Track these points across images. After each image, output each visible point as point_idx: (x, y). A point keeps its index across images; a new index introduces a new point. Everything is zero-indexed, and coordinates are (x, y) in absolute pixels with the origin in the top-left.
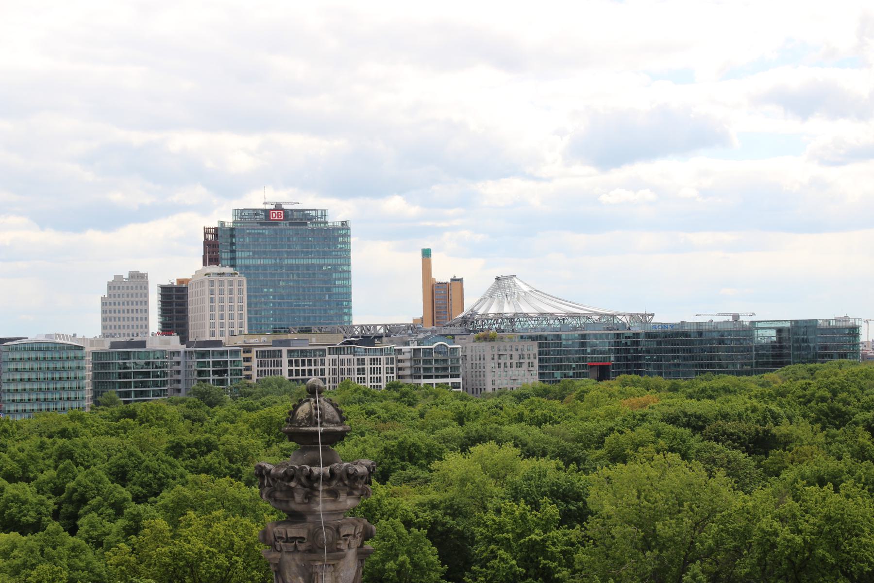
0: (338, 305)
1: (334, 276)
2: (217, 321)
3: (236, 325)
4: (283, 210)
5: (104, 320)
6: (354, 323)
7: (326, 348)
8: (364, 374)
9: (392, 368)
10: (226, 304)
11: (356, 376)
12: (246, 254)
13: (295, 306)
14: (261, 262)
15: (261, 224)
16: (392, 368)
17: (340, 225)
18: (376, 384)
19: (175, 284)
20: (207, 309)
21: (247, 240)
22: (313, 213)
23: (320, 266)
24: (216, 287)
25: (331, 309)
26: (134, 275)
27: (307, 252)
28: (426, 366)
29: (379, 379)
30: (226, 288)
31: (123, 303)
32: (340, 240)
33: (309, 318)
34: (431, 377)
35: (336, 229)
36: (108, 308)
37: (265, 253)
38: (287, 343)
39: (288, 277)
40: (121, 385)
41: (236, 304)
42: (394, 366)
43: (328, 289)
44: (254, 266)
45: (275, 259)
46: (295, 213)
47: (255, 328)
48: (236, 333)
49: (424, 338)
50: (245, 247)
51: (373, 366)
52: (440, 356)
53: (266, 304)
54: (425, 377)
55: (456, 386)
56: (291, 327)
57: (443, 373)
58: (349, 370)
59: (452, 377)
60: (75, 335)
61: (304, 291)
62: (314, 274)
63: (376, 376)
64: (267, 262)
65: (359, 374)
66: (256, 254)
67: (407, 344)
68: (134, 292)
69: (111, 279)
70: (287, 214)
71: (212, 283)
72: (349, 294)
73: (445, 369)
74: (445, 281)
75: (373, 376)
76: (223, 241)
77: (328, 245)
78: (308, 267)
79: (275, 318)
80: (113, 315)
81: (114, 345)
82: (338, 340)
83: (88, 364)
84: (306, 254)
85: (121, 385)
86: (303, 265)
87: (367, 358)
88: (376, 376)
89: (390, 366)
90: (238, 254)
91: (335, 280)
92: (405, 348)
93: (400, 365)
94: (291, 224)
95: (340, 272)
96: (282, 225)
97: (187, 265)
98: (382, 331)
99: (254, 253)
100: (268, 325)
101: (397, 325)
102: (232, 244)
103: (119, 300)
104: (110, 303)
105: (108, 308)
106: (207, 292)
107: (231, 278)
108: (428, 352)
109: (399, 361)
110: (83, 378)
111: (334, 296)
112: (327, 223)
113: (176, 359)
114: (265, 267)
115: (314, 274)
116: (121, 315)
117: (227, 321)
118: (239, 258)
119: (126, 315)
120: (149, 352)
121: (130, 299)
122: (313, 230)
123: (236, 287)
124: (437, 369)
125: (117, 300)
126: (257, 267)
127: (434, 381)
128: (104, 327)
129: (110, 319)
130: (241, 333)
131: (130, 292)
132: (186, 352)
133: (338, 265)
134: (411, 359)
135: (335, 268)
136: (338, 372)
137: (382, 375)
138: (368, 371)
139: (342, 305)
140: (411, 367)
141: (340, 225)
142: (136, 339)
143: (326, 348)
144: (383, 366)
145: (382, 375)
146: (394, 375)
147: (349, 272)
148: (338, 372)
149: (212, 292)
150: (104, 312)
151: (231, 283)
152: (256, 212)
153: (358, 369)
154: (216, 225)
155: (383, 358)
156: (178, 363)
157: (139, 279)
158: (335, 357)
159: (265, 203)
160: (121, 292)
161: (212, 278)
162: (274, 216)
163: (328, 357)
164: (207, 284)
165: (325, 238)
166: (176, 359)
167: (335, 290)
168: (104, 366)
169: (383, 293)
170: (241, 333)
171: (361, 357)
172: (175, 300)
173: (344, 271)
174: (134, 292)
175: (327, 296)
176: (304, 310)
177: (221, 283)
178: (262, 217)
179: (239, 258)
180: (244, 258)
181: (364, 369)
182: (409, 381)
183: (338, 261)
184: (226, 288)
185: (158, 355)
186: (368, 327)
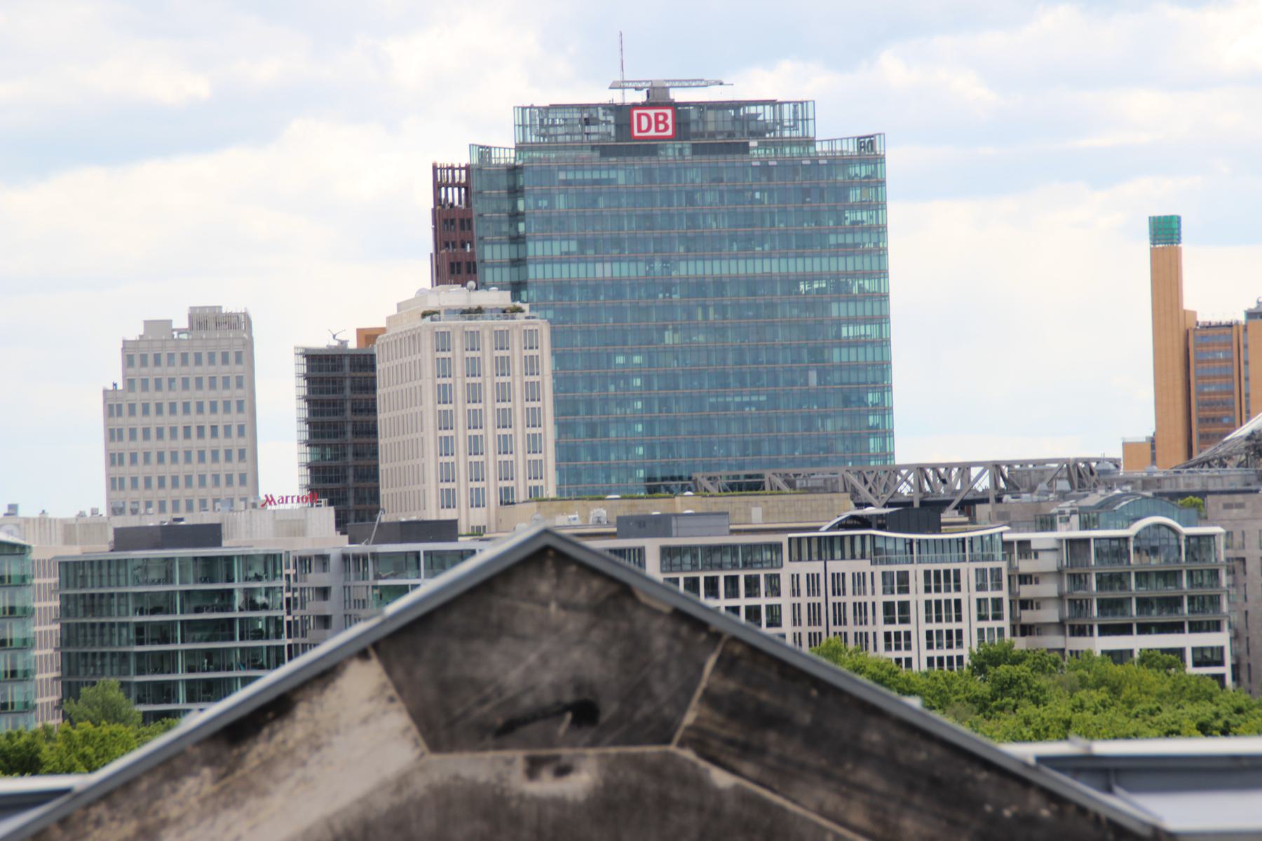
0: (846, 401)
1: (836, 310)
2: (461, 460)
3: (521, 471)
4: (673, 105)
5: (114, 459)
6: (900, 459)
7: (783, 539)
8: (905, 621)
9: (997, 603)
10: (489, 406)
11: (882, 628)
12: (557, 248)
13: (714, 407)
14: (604, 271)
15: (605, 151)
16: (997, 603)
17: (851, 148)
18: (945, 653)
19: (352, 345)
20: (430, 421)
21: (561, 203)
22: (767, 114)
23: (791, 282)
24: (458, 354)
25: (825, 417)
26: (204, 320)
27: (749, 239)
28: (1108, 595)
29: (955, 638)
30: (488, 354)
31: (173, 408)
32: (855, 195)
33: (758, 444)
34: (1125, 630)
35: (838, 162)
36: (124, 422)
37: (617, 242)
38: (660, 526)
39: (690, 316)
40: (145, 663)
41: (518, 406)
42: (1004, 594)
43: (817, 354)
44: (584, 285)
45: (650, 262)
46: (711, 115)
47: (578, 482)
48: (521, 495)
49: (1102, 506)
50: (554, 225)
51: (933, 596)
52: (1155, 563)
53: (623, 402)
54: (1105, 630)
55: (1206, 657)
56: (697, 475)
57: (1166, 618)
58: (860, 609)
59: (1196, 627)
60: (13, 509)
61: (741, 362)
62: (772, 306)
63: (944, 626)
64: (625, 270)
65: (889, 621)
66: (590, 248)
67: (1047, 523)
68: (205, 370)
69: (135, 331)
70: (685, 119)
71: (443, 340)
72: (883, 367)
73: (1173, 603)
74: (1225, 318)
75: (934, 626)
76: (488, 210)
77: (816, 215)
78: (752, 284)
79: (650, 448)
80: (139, 445)
81: (125, 538)
82: (827, 514)
83: (44, 600)
84: (747, 245)
85: (145, 663)
86: (736, 279)
87: (916, 572)
88: (944, 626)
89: (990, 594)
90: (534, 249)
91: (839, 323)
92: (1040, 539)
93: (1026, 591)
94: (696, 150)
95: (855, 299)
96: (670, 152)
97: (374, 281)
98: (984, 484)
99: (582, 243)
100: (630, 471)
101: (1036, 463)
102: (516, 216)
103: (212, 395)
104: (132, 407)
105: (124, 422)
106: (429, 370)
107: (502, 324)
108: (1117, 549)
109: (1025, 579)
110: (26, 644)
111: (836, 376)
112: (810, 142)
113: (316, 578)
114: (616, 287)
115: (772, 306)
116: (167, 444)
117: (491, 458)
118: (536, 261)
119: (180, 444)
120: (229, 560)
121: (193, 395)
122: (765, 169)
123: (517, 353)
124: (1144, 603)
125: (153, 397)
126: (592, 288)
127: (1136, 643)
128: (114, 483)
129: (134, 458)
130: (535, 495)
131: (193, 371)
132: (345, 558)
133: (847, 275)
134: (1060, 572)
135: (839, 287)
136: (827, 614)
137: (963, 625)
138: (917, 613)
139: (862, 401)
140: (1061, 597)
141: (851, 148)
142: (190, 519)
143: (783, 539)
144: (968, 595)
145: (963, 625)
146: (1005, 623)
147: (883, 297)
148: (827, 614)
149: (444, 368)
150: (113, 435)
151: (502, 340)
152: (587, 114)
153: (888, 607)
154: (462, 158)
155: (968, 570)
156: (324, 592)
157: (221, 339)
158: (816, 567)
160: (164, 371)
161: (444, 324)
162: (644, 126)
163: (788, 570)
164: (428, 343)
165: (806, 192)
166: (316, 578)
167: (837, 356)
168: (93, 604)
170: (535, 495)
171: (895, 568)
172: (341, 390)
173: (865, 296)
174: (205, 370)
175: (813, 377)
176: (743, 420)
177: (473, 341)
178: (606, 128)
179: (536, 261)
180: (552, 260)
181: (904, 606)
182: (1054, 641)
183: (850, 264)
184: (488, 354)
185: (258, 569)
186: (941, 473)
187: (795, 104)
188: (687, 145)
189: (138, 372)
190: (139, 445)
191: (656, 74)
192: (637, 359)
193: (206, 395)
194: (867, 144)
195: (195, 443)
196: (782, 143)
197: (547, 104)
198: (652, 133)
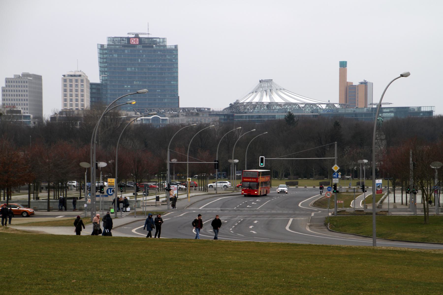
4: (139, 38)
17: (174, 47)
22: (158, 40)
46: (146, 40)
112: (166, 46)
116: (13, 98)
119: (15, 98)
121: (18, 89)
125: (11, 89)
141: (174, 47)
159: (128, 34)
162: (133, 42)
169: (211, 110)
173: (103, 58)
174: (20, 84)
184: (74, 83)
187: (163, 39)
188: (141, 45)
189: (8, 84)
190: (8, 97)
191: (137, 32)
192: (129, 86)
193: (20, 89)
194: (176, 47)
195: (18, 98)
196: (160, 46)
197: (114, 36)
198: (134, 43)
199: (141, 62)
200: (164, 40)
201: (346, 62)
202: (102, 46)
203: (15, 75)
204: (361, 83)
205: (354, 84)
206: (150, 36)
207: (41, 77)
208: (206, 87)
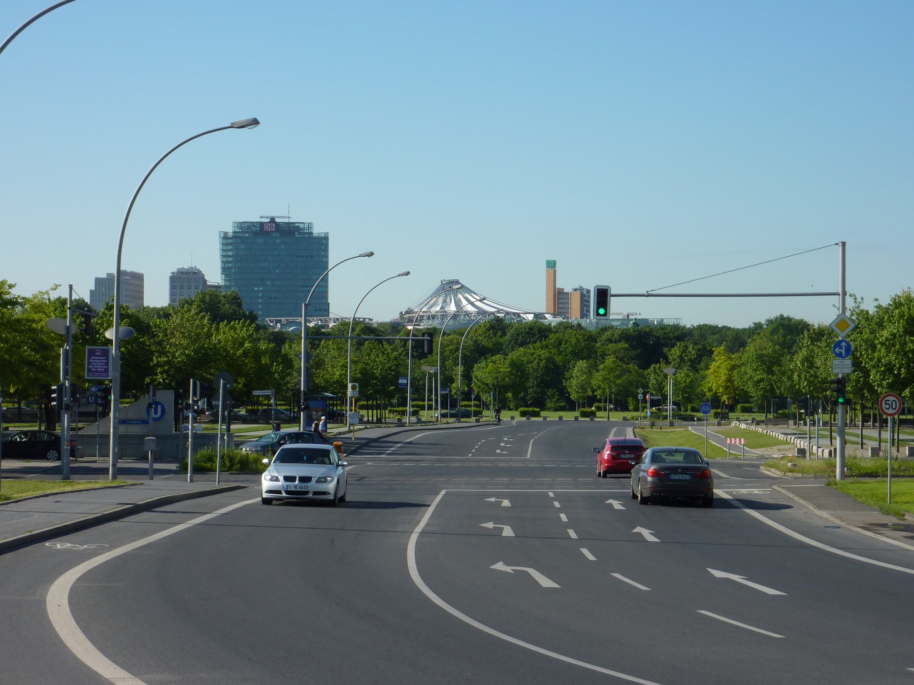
4: (276, 223)
22: (302, 226)
162: (267, 228)
199: (280, 254)
200: (310, 226)
201: (547, 262)
202: (225, 234)
203: (108, 274)
204: (576, 290)
205: (565, 291)
206: (291, 221)
207: (142, 275)
208: (360, 292)
